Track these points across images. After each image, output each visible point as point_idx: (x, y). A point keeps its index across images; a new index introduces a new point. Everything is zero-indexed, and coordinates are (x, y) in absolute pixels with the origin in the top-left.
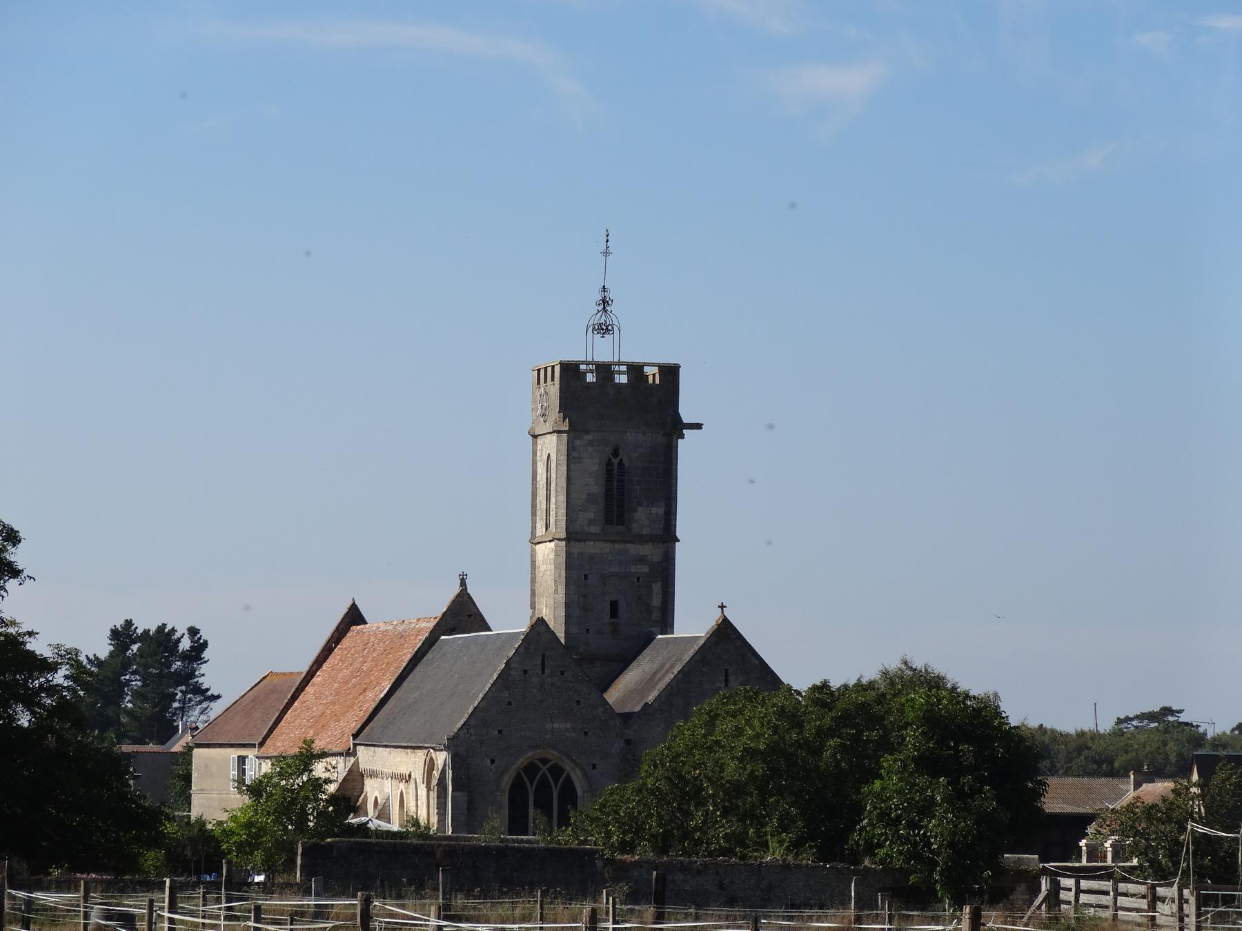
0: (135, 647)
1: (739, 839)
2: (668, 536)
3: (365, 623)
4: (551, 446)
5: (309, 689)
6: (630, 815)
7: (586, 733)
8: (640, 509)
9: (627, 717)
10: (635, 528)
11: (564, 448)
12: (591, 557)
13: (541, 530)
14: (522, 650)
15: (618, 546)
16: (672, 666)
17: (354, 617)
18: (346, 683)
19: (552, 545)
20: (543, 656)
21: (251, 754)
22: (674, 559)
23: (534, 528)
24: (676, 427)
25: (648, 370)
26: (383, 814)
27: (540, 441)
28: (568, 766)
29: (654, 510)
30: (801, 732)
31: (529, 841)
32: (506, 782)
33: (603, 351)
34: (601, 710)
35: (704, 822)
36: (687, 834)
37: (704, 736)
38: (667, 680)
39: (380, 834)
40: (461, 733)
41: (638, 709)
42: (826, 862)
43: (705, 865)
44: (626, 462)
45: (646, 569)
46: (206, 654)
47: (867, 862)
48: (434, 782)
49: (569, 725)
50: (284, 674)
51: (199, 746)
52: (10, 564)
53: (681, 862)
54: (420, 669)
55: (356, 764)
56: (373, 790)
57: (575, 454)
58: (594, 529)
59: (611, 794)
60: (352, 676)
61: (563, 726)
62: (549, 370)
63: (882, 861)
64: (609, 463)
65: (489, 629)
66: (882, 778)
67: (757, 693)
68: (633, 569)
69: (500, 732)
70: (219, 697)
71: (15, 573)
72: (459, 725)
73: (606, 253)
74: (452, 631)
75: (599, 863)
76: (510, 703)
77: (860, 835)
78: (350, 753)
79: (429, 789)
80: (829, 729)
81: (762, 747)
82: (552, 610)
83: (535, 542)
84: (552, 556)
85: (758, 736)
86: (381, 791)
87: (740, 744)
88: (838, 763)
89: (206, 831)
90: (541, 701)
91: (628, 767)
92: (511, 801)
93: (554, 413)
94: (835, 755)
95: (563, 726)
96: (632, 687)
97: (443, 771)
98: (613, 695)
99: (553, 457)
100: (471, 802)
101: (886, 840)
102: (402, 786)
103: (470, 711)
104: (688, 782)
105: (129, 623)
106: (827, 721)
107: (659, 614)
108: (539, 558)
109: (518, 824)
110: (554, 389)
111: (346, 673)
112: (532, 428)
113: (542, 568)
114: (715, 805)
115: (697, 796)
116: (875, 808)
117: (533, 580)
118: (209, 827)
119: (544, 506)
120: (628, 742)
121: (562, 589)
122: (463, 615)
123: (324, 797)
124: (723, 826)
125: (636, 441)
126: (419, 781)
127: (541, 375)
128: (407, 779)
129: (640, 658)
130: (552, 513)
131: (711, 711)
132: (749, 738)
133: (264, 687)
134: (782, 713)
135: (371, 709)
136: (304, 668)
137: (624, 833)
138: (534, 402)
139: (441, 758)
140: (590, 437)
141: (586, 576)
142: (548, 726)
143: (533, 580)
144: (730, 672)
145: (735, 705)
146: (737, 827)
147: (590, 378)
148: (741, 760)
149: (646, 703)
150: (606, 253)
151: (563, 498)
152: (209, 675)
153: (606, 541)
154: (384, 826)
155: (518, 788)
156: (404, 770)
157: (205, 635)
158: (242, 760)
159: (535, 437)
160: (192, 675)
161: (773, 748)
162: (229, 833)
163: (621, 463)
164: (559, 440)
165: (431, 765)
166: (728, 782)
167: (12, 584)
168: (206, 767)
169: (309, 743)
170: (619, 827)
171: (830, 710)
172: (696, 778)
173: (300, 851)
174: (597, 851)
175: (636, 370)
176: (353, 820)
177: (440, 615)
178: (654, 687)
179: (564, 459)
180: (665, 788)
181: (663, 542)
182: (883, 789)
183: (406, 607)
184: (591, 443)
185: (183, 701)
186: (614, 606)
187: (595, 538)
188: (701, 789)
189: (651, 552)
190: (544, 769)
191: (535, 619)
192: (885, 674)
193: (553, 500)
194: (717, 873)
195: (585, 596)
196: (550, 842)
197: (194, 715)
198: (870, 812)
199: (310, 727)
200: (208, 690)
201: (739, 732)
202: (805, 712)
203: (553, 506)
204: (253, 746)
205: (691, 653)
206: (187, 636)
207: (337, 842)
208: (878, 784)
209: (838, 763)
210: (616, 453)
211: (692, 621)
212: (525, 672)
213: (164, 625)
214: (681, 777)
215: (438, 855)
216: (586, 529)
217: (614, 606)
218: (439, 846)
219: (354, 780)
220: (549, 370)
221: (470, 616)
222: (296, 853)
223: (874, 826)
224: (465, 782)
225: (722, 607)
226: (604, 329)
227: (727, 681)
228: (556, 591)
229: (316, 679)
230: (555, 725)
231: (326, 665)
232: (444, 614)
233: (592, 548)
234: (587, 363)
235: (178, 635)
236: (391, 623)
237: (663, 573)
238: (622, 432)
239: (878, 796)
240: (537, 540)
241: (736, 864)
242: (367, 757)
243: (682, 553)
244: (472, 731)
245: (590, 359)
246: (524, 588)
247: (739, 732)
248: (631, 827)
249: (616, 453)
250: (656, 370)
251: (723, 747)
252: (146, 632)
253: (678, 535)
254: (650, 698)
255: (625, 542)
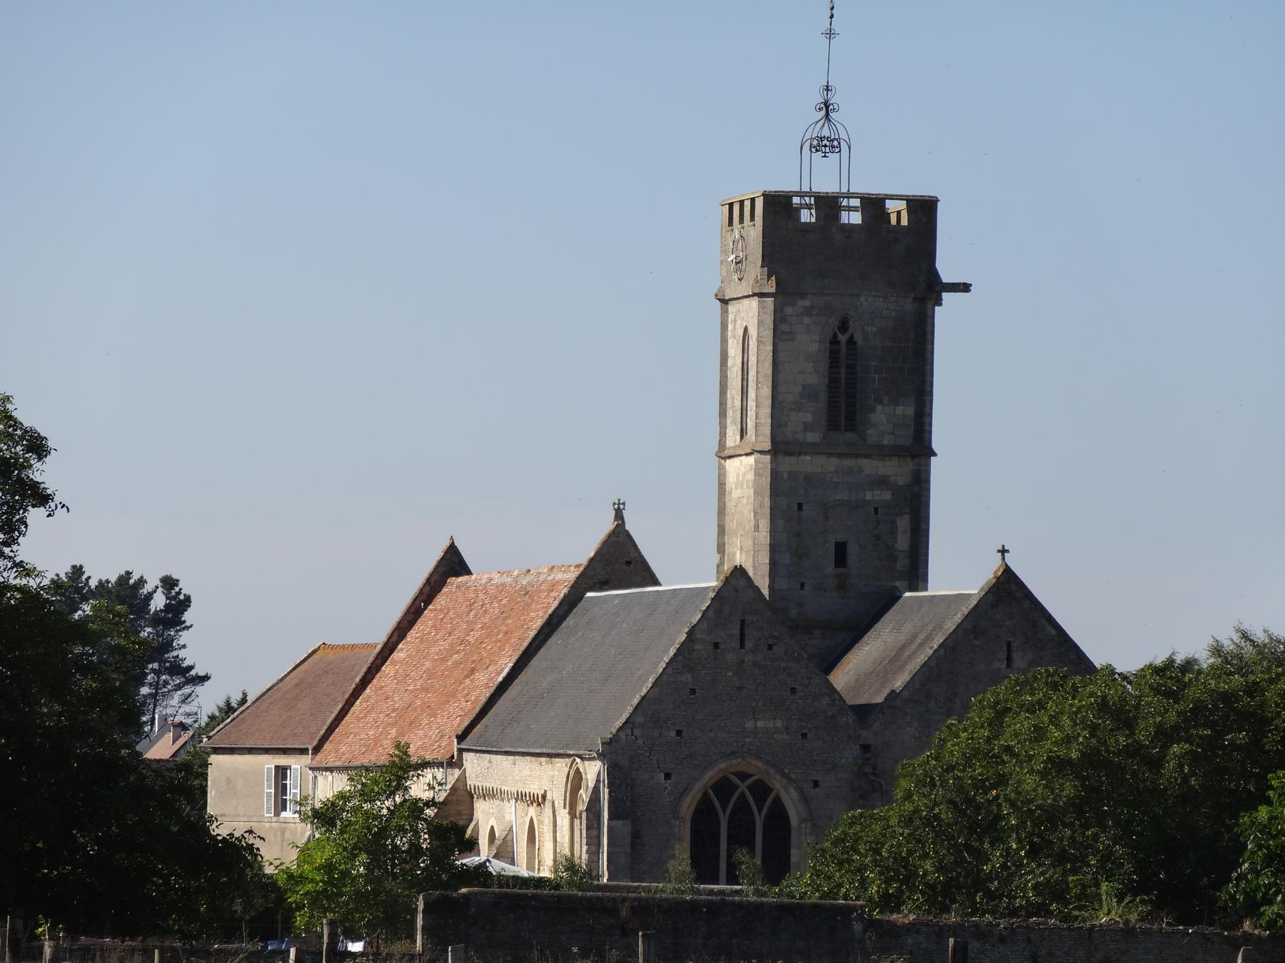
0: (87, 608)
1: (1056, 892)
2: (919, 447)
3: (469, 573)
4: (750, 316)
5: (387, 669)
6: (897, 858)
7: (804, 736)
8: (879, 407)
9: (864, 712)
10: (872, 435)
11: (769, 319)
12: (809, 478)
13: (732, 438)
14: (711, 613)
15: (848, 463)
16: (929, 637)
17: (452, 564)
18: (444, 660)
19: (751, 460)
20: (743, 622)
21: (297, 764)
22: (928, 481)
23: (723, 434)
24: (932, 288)
25: (891, 206)
26: (504, 851)
27: (732, 308)
28: (777, 784)
29: (900, 410)
30: (1133, 734)
31: (722, 892)
32: (688, 806)
33: (825, 177)
34: (826, 701)
35: (1004, 866)
36: (979, 883)
37: (989, 740)
38: (922, 658)
39: (504, 880)
40: (622, 735)
41: (879, 699)
42: (1188, 924)
43: (1011, 930)
44: (858, 338)
45: (887, 496)
46: (188, 617)
47: (1247, 926)
48: (582, 807)
49: (779, 724)
50: (343, 647)
51: (217, 751)
52: (35, 486)
53: (977, 925)
54: (555, 641)
55: (462, 778)
56: (486, 818)
57: (785, 327)
58: (813, 437)
59: (851, 825)
60: (452, 650)
61: (770, 724)
62: (747, 204)
63: (1271, 925)
64: (834, 341)
65: (655, 582)
66: (1268, 802)
67: (1064, 677)
68: (869, 496)
69: (679, 733)
70: (206, 678)
71: (41, 498)
72: (619, 723)
73: (830, 34)
74: (603, 585)
75: (858, 927)
76: (693, 691)
77: (1237, 886)
78: (453, 762)
79: (573, 815)
80: (1176, 728)
81: (1074, 755)
82: (749, 550)
83: (724, 455)
84: (751, 476)
85: (1068, 740)
86: (500, 817)
87: (1043, 751)
88: (1185, 779)
89: (265, 875)
90: (740, 689)
91: (870, 785)
92: (695, 833)
93: (755, 268)
94: (1181, 766)
95: (770, 724)
96: (872, 666)
97: (596, 789)
98: (841, 678)
99: (753, 332)
100: (636, 835)
101: (1276, 894)
102: (532, 811)
103: (636, 701)
104: (978, 808)
105: (77, 571)
106: (1172, 717)
107: (907, 562)
108: (731, 479)
109: (704, 868)
110: (754, 232)
111: (443, 645)
112: (721, 289)
113: (736, 494)
114: (1019, 841)
115: (992, 828)
116: (1260, 847)
117: (722, 511)
118: (269, 870)
119: (738, 403)
120: (866, 748)
121: (765, 524)
122: (619, 562)
123: (986, 845)
124: (1032, 872)
125: (874, 308)
126: (559, 803)
127: (735, 212)
128: (539, 801)
129: (879, 625)
130: (751, 413)
131: (997, 703)
132: (1056, 743)
133: (314, 668)
134: (1103, 706)
135: (483, 700)
136: (379, 637)
137: (888, 882)
138: (724, 252)
139: (593, 770)
140: (807, 303)
141: (800, 506)
142: (750, 724)
143: (722, 511)
144: (1014, 646)
145: (1032, 694)
146: (1054, 874)
147: (807, 216)
148: (1043, 774)
149: (893, 692)
150: (830, 34)
151: (767, 391)
152: (193, 647)
153: (830, 455)
154: (510, 870)
155: (704, 813)
156: (535, 789)
157: (186, 587)
158: (281, 772)
159: (725, 302)
160: (168, 646)
161: (1091, 759)
162: (294, 879)
163: (851, 341)
164: (761, 307)
165: (576, 780)
166: (1039, 807)
167: (35, 515)
168: (228, 781)
169: (402, 749)
170: (881, 873)
171: (1176, 702)
172: (990, 802)
173: (421, 907)
174: (854, 908)
175: (874, 205)
176: (470, 861)
177: (584, 561)
178: (901, 669)
179: (769, 334)
180: (945, 813)
181: (913, 457)
182: (1272, 818)
183: (535, 550)
184: (807, 312)
185: (156, 685)
186: (841, 549)
187: (814, 450)
188: (999, 817)
189: (894, 470)
190: (743, 787)
191: (727, 567)
192: (1217, 650)
193: (752, 394)
194: (1029, 941)
195: (798, 535)
196: (780, 894)
197: (172, 707)
198: (1253, 853)
199: (392, 725)
200: (191, 668)
201: (1039, 734)
202: (1137, 707)
203: (751, 403)
204: (303, 751)
205: (958, 618)
206: (160, 589)
207: (475, 894)
208: (1263, 813)
209: (1185, 779)
210: (844, 326)
211: (956, 570)
212: (716, 645)
213: (128, 573)
214: (970, 801)
215: (624, 913)
216: (800, 437)
217: (841, 549)
218: (624, 900)
219: (458, 803)
220: (747, 204)
221: (628, 563)
222: (416, 909)
223: (1258, 874)
224: (628, 804)
225: (1003, 551)
226: (825, 145)
227: (1009, 660)
228: (757, 528)
229: (398, 655)
230: (760, 724)
231: (413, 635)
232: (592, 561)
233: (809, 464)
234: (801, 194)
235: (148, 588)
236: (509, 573)
237: (914, 501)
238: (853, 301)
239: (1264, 829)
240: (727, 453)
241: (1056, 928)
242: (478, 769)
243: (937, 466)
244: (637, 732)
245: (806, 189)
246: (709, 520)
247: (1039, 734)
248: (897, 872)
249: (844, 326)
250: (902, 205)
251: (1017, 755)
252: (102, 585)
253: (935, 446)
254: (898, 684)
255: (857, 456)
